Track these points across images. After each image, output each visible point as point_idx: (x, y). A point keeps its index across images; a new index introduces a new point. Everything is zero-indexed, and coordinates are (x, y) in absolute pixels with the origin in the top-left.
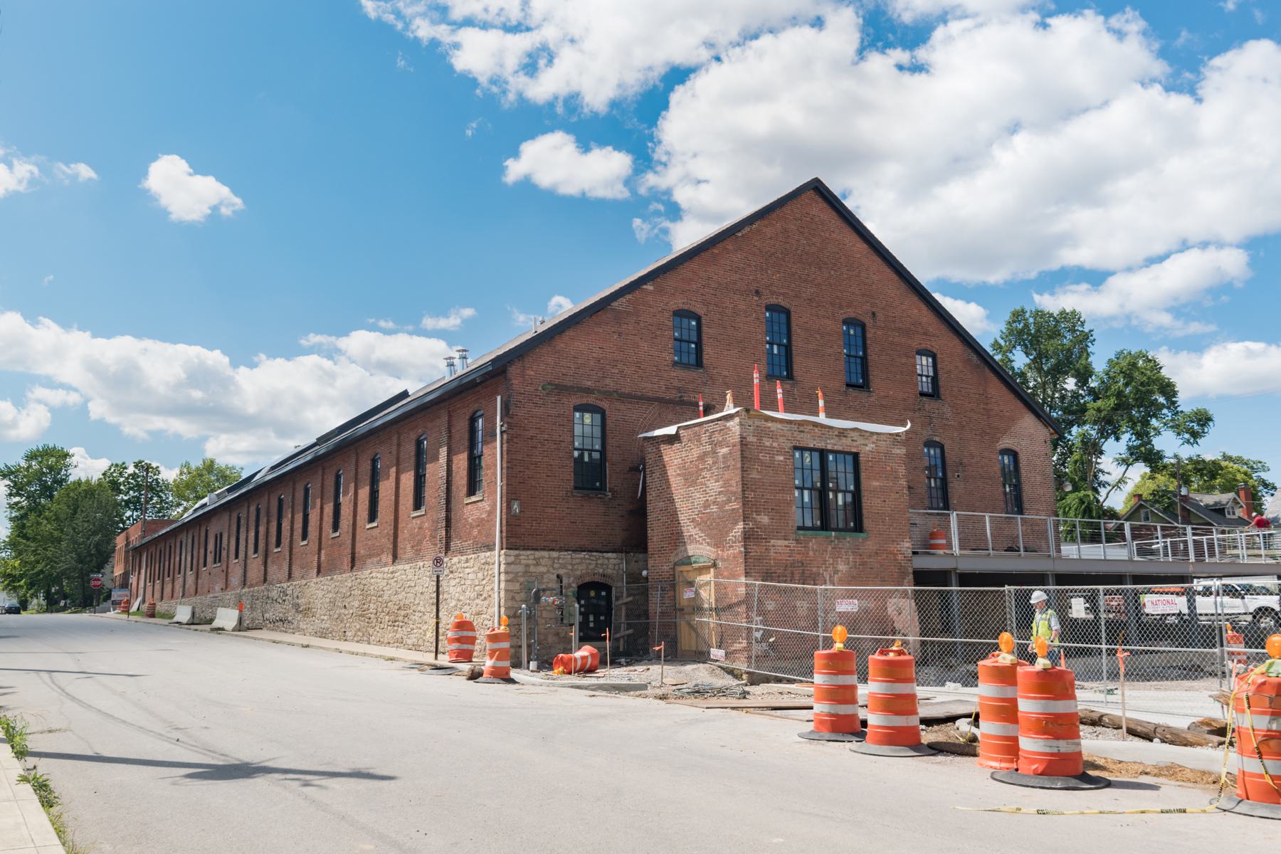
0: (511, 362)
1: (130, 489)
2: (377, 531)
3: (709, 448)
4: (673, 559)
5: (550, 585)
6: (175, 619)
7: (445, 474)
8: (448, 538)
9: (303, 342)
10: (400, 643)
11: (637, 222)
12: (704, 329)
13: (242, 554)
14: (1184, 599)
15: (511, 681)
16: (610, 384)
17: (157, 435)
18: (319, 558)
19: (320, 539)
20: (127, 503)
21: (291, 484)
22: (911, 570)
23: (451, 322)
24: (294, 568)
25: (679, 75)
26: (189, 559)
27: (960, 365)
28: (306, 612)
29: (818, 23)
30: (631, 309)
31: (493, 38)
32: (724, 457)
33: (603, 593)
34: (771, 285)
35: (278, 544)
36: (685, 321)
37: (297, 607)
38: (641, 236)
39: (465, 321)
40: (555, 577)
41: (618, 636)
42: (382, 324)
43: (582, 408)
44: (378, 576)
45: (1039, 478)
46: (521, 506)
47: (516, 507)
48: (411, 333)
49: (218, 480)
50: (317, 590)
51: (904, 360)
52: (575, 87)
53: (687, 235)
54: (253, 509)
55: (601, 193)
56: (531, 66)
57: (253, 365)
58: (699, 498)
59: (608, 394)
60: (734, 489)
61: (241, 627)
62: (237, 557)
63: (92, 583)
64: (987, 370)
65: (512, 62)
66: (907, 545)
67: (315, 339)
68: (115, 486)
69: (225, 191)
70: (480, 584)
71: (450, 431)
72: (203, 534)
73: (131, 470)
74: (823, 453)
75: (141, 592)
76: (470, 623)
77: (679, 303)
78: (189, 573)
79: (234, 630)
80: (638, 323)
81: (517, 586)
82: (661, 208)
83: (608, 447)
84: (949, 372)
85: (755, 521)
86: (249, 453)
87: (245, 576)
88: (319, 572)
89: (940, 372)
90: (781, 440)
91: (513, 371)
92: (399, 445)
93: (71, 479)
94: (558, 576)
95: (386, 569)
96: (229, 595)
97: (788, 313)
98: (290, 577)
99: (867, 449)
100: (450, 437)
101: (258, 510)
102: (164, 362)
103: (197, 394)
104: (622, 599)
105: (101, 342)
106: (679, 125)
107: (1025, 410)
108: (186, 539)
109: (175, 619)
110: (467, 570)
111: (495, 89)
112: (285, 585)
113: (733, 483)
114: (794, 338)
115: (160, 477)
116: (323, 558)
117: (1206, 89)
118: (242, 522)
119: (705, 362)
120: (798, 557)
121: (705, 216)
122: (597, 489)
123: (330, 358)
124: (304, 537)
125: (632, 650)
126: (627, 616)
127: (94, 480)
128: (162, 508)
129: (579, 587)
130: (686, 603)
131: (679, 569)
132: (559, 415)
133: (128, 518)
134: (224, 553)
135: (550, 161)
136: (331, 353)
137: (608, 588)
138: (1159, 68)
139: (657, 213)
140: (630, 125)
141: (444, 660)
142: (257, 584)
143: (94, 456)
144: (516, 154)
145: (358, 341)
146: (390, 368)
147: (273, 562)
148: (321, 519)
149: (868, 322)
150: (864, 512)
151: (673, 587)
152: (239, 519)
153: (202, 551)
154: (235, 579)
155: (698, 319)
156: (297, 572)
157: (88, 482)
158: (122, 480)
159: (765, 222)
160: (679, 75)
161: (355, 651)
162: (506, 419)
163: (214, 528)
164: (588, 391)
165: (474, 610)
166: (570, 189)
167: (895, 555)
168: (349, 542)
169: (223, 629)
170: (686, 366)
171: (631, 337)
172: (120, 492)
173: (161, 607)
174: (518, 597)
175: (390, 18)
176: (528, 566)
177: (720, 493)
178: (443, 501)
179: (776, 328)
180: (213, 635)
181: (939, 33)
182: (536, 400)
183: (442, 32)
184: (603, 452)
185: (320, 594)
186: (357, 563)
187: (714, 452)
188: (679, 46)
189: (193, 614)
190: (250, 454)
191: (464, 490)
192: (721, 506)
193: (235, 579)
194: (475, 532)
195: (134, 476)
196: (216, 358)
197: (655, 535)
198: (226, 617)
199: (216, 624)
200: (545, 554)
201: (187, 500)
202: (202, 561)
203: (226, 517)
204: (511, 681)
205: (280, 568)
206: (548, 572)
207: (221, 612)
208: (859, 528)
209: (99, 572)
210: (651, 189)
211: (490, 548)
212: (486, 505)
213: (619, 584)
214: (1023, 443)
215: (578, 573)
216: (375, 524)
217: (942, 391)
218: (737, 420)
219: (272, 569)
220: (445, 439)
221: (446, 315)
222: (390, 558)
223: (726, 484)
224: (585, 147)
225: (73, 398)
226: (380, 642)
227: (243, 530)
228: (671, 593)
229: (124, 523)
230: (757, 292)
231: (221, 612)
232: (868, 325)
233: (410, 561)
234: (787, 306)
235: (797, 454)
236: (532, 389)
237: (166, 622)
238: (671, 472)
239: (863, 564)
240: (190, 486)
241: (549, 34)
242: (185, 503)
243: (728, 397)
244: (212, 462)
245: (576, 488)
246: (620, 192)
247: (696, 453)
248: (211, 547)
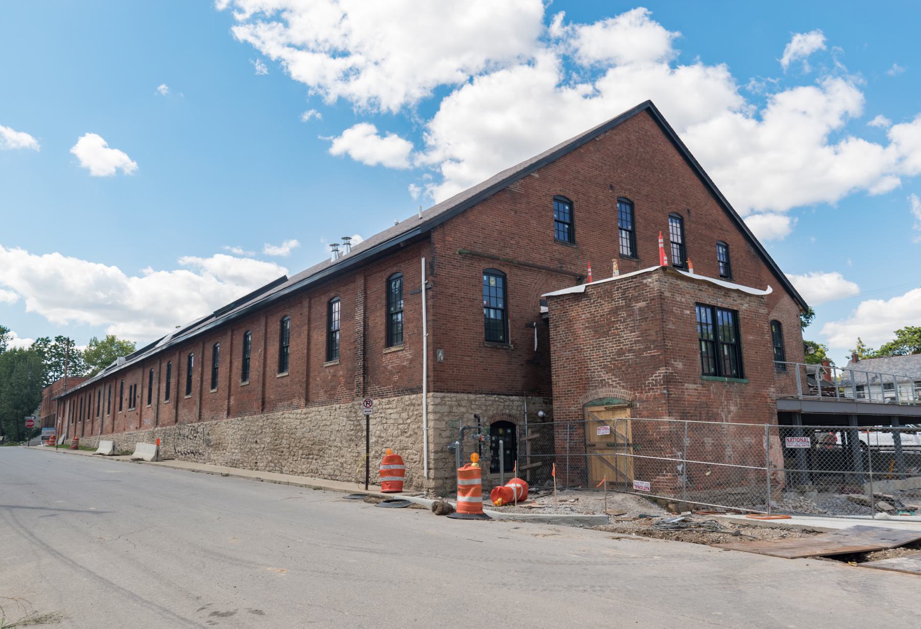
0: (434, 229)
1: (52, 356)
2: (288, 379)
3: (622, 303)
4: (582, 400)
5: (469, 424)
6: (98, 451)
7: (361, 329)
8: (366, 383)
9: (180, 262)
10: (314, 473)
11: (412, 187)
12: (576, 213)
13: (154, 401)
14: (890, 435)
15: (485, 517)
16: (509, 253)
17: (73, 322)
18: (229, 402)
19: (230, 387)
20: (50, 366)
21: (201, 344)
22: (776, 412)
23: (283, 251)
24: (204, 411)
25: (444, 91)
26: (106, 405)
27: (743, 254)
28: (217, 446)
29: (531, 63)
30: (523, 192)
31: (320, 59)
32: (640, 309)
33: (509, 431)
34: (621, 181)
35: (189, 391)
36: (561, 205)
37: (208, 443)
38: (415, 196)
39: (292, 250)
40: (472, 416)
41: (524, 467)
42: (235, 250)
43: (488, 273)
44: (293, 419)
45: (795, 343)
46: (444, 354)
47: (440, 355)
48: (255, 258)
49: (117, 351)
50: (229, 429)
51: (709, 248)
52: (373, 93)
53: (445, 194)
54: (164, 365)
55: (390, 163)
56: (348, 75)
57: (141, 276)
58: (611, 347)
59: (510, 263)
60: (654, 338)
61: (158, 457)
62: (149, 402)
63: (27, 423)
64: (760, 261)
65: (331, 76)
66: (773, 390)
67: (188, 260)
68: (41, 353)
69: (125, 157)
70: (411, 423)
71: (366, 293)
72: (119, 386)
73: (53, 343)
74: (713, 309)
75: (65, 430)
76: (399, 458)
77: (557, 190)
78: (106, 415)
79: (152, 460)
80: (528, 203)
81: (442, 425)
82: (430, 177)
83: (510, 307)
84: (737, 260)
85: (672, 366)
86: (135, 336)
87: (157, 418)
88: (228, 414)
89: (732, 260)
90: (687, 296)
91: (436, 236)
92: (310, 307)
93: (8, 349)
94: (475, 416)
95: (299, 411)
96: (143, 433)
97: (632, 205)
98: (200, 418)
99: (743, 307)
100: (366, 298)
101: (169, 366)
102: (79, 273)
103: (101, 295)
104: (527, 435)
105: (34, 258)
106: (446, 123)
107: (784, 292)
108: (104, 390)
109: (98, 451)
110: (390, 411)
111: (321, 92)
112: (196, 425)
113: (653, 332)
114: (637, 225)
115: (75, 347)
116: (232, 402)
117: (772, 114)
118: (154, 375)
119: (577, 239)
120: (703, 399)
121: (460, 182)
122: (501, 342)
123: (197, 272)
124: (214, 384)
125: (538, 482)
126: (532, 450)
127: (26, 348)
128: (76, 370)
129: (491, 425)
130: (597, 440)
131: (590, 409)
132: (472, 277)
133: (51, 377)
134: (138, 400)
135: (360, 143)
136: (198, 270)
137: (512, 426)
138: (738, 101)
139: (428, 181)
140: (412, 121)
141: (375, 490)
142: (168, 424)
143: (22, 337)
144: (339, 134)
145: (218, 262)
146: (239, 280)
147: (184, 407)
148: (231, 371)
149: (686, 216)
150: (745, 361)
151: (583, 425)
152: (151, 373)
153: (118, 399)
154: (148, 419)
155: (571, 204)
156: (206, 413)
157: (21, 350)
158: (46, 350)
159: (615, 131)
160: (444, 91)
161: (278, 480)
162: (431, 278)
163: (128, 381)
164: (493, 258)
165: (397, 445)
166: (371, 162)
167: (766, 398)
168: (260, 389)
169: (142, 460)
170: (563, 243)
171: (524, 215)
172: (45, 358)
173: (83, 441)
174: (444, 434)
175: (251, 40)
176: (451, 407)
177: (636, 342)
178: (360, 352)
179: (624, 217)
180: (135, 464)
181: (611, 73)
182: (454, 262)
183: (286, 53)
184: (504, 311)
185: (231, 432)
186: (268, 406)
187: (628, 306)
188: (445, 70)
189: (114, 447)
190: (138, 334)
191: (383, 342)
192: (638, 353)
193: (148, 419)
194: (396, 378)
195: (55, 347)
196: (113, 271)
197: (561, 379)
198: (146, 450)
199: (136, 455)
200: (465, 396)
201: (95, 364)
202: (118, 406)
203: (139, 373)
204: (485, 517)
205: (190, 411)
206: (467, 412)
207: (139, 446)
208: (740, 374)
209: (30, 415)
210: (423, 163)
211: (418, 390)
212: (408, 354)
213: (521, 423)
214: (785, 316)
215: (491, 413)
216: (285, 374)
217: (733, 273)
218: (655, 276)
219: (183, 412)
220: (362, 299)
221: (280, 245)
222: (303, 402)
223: (644, 333)
224: (382, 134)
225: (11, 297)
226: (293, 472)
227: (155, 381)
228: (581, 431)
229: (48, 381)
230: (612, 187)
231: (139, 446)
232: (686, 219)
233: (323, 404)
234: (632, 199)
235: (697, 309)
236: (451, 253)
237: (90, 453)
238: (578, 326)
239: (747, 405)
240: (97, 354)
241: (355, 60)
242: (93, 367)
243: (615, 266)
244: (113, 338)
245: (486, 340)
246: (404, 164)
247: (607, 307)
248: (126, 395)
